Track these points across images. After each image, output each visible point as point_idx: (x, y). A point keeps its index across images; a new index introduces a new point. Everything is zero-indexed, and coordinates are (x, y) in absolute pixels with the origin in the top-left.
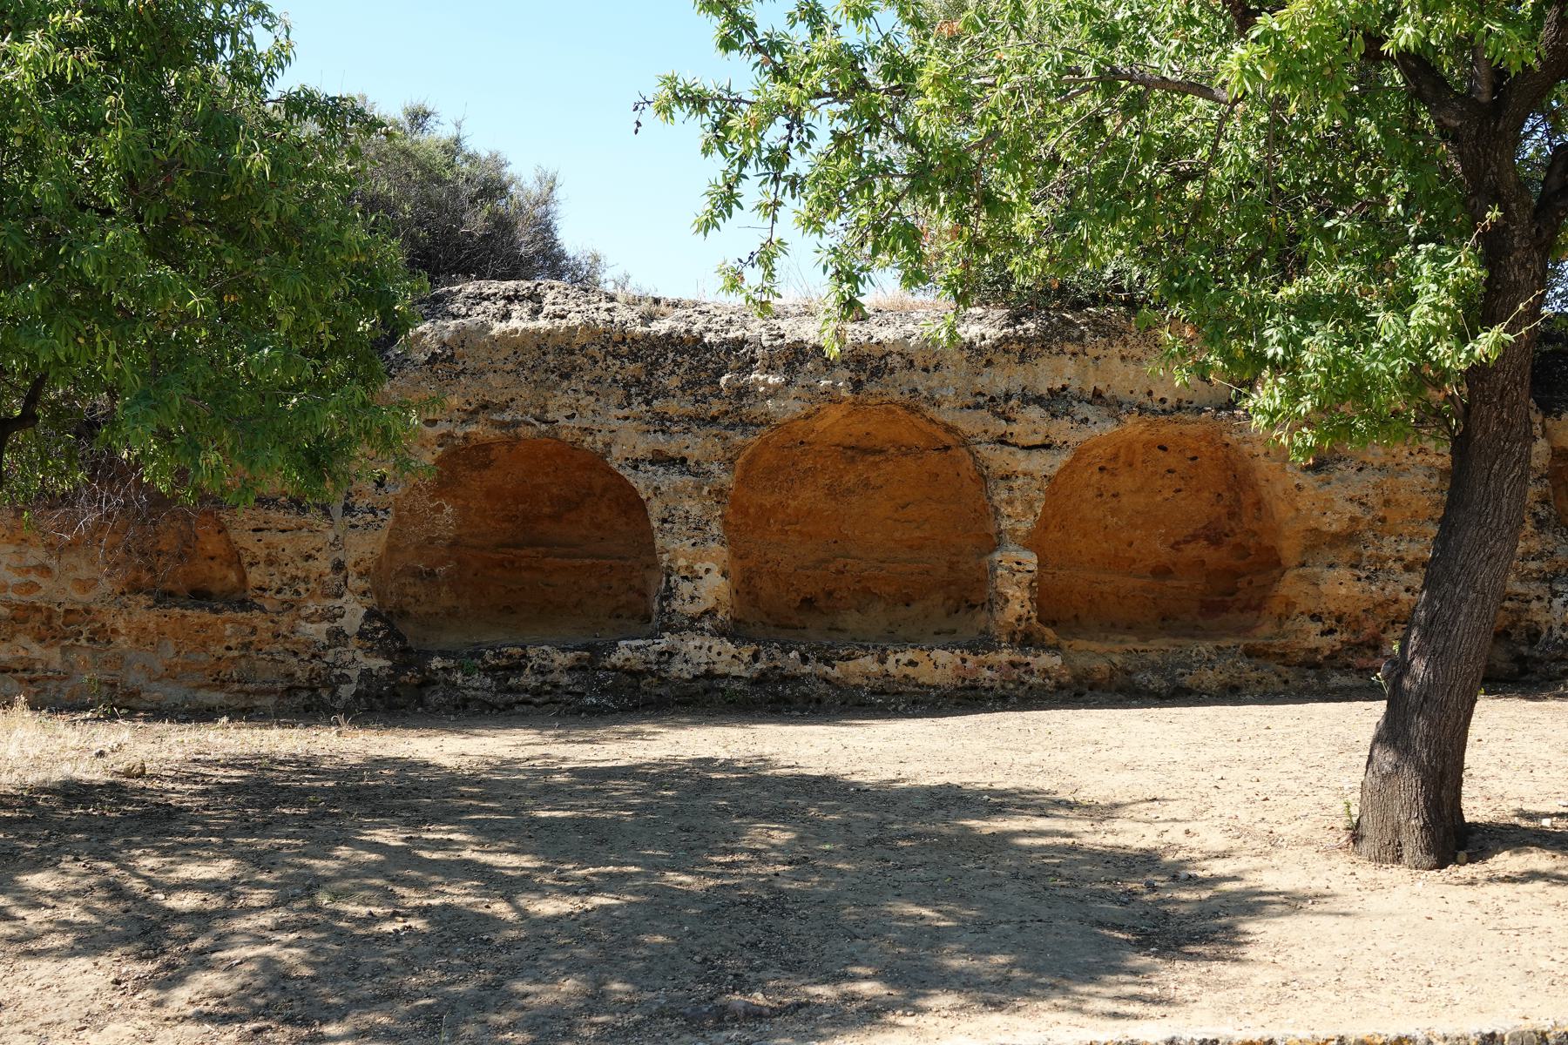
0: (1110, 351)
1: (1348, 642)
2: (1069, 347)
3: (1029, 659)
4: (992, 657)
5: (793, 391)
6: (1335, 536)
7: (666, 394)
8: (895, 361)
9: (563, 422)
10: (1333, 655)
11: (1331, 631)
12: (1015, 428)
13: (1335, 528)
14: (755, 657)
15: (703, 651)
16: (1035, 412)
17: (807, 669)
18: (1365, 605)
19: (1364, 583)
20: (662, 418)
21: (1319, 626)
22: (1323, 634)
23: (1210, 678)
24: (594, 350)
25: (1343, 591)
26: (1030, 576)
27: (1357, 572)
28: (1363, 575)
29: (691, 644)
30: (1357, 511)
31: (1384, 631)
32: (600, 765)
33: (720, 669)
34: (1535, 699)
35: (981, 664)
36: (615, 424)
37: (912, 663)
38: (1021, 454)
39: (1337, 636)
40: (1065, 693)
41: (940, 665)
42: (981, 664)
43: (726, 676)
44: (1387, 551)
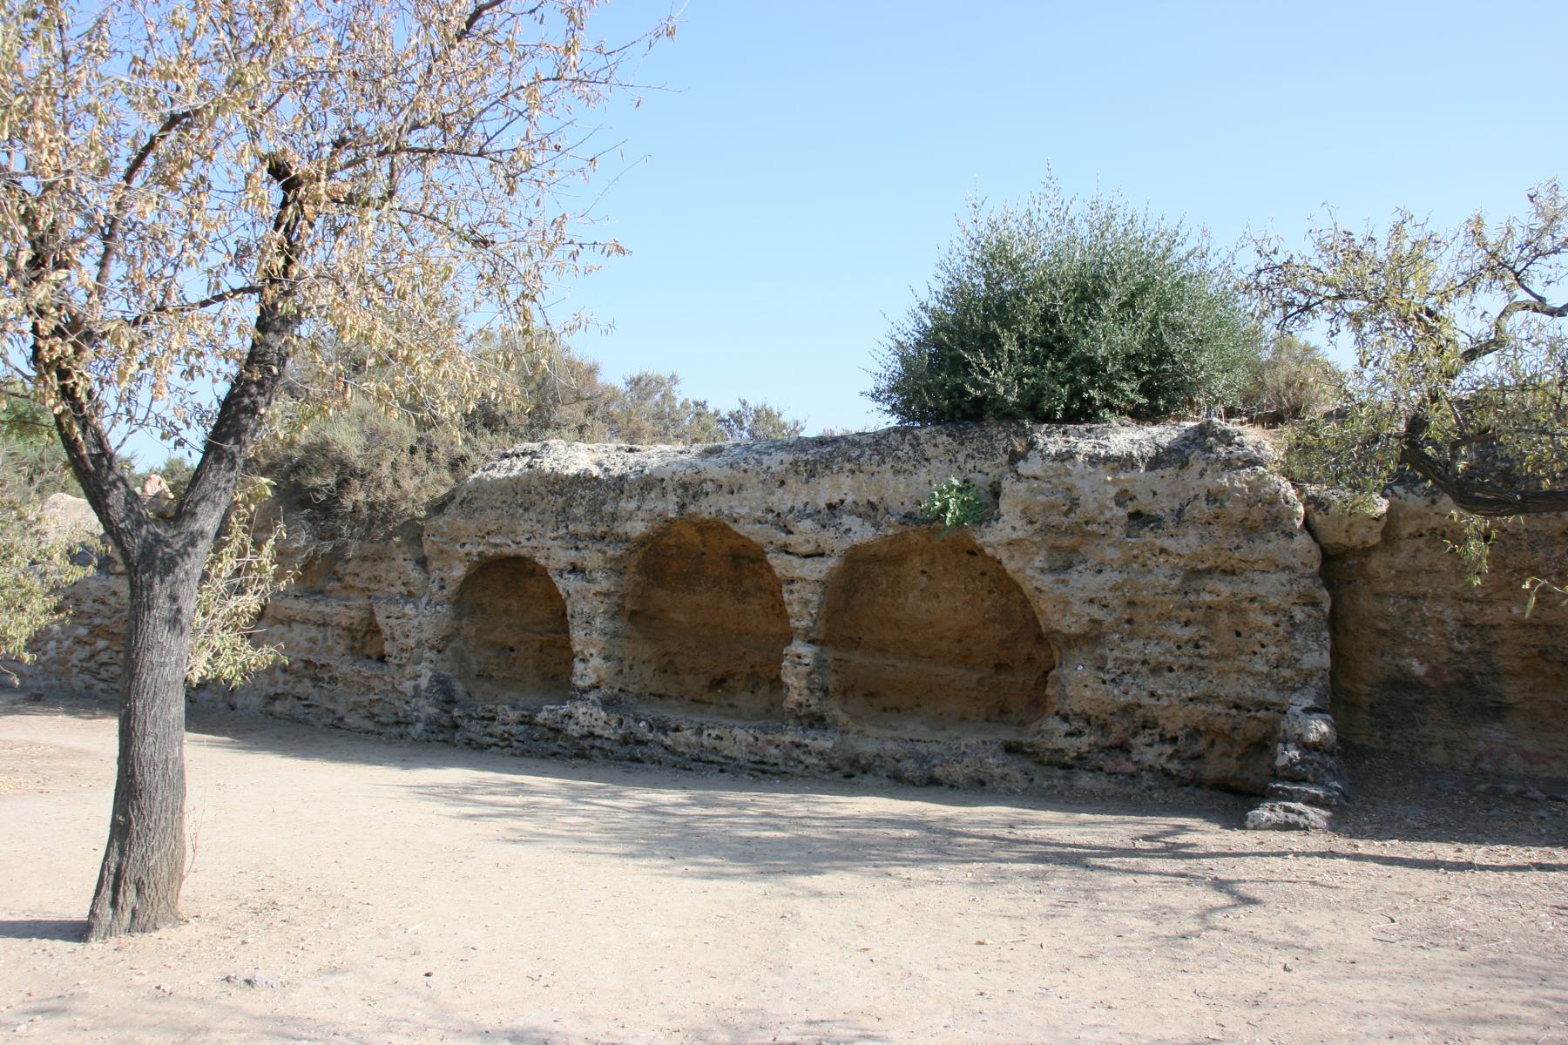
0: (884, 467)
1: (1096, 745)
2: (848, 466)
3: (807, 741)
4: (779, 738)
5: (641, 514)
6: (1076, 637)
7: (575, 519)
8: (709, 487)
9: (524, 542)
10: (1080, 757)
11: (1079, 733)
12: (791, 539)
13: (1074, 629)
14: (621, 722)
15: (587, 716)
16: (807, 524)
17: (650, 736)
18: (1109, 709)
19: (1109, 686)
20: (575, 536)
21: (1065, 727)
22: (1070, 734)
23: (957, 771)
24: (542, 489)
25: (1088, 693)
26: (807, 669)
27: (1101, 674)
28: (1107, 677)
29: (580, 710)
30: (1097, 613)
31: (1135, 734)
32: (1535, 854)
33: (598, 731)
34: (406, 768)
35: (769, 743)
36: (549, 543)
37: (719, 738)
38: (796, 561)
39: (1085, 739)
40: (837, 774)
41: (739, 739)
42: (769, 743)
43: (600, 737)
44: (1133, 656)
